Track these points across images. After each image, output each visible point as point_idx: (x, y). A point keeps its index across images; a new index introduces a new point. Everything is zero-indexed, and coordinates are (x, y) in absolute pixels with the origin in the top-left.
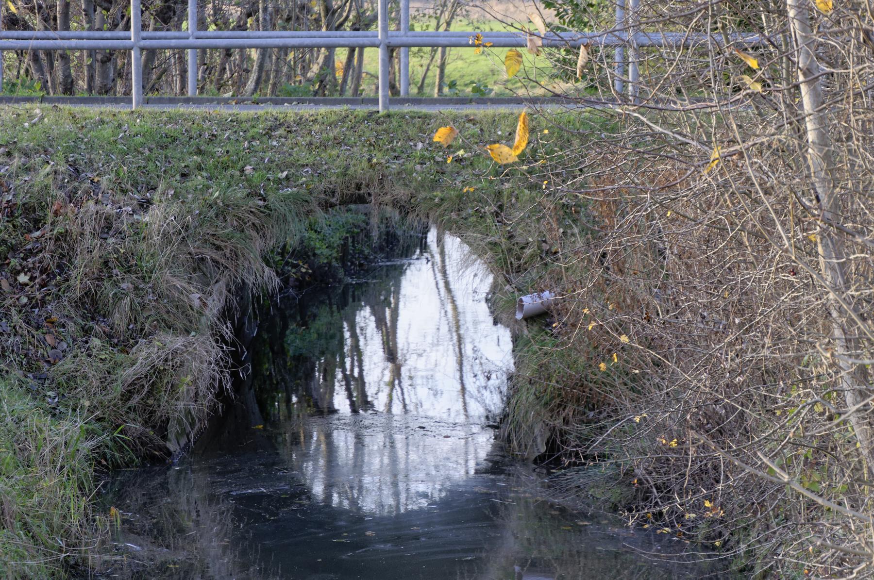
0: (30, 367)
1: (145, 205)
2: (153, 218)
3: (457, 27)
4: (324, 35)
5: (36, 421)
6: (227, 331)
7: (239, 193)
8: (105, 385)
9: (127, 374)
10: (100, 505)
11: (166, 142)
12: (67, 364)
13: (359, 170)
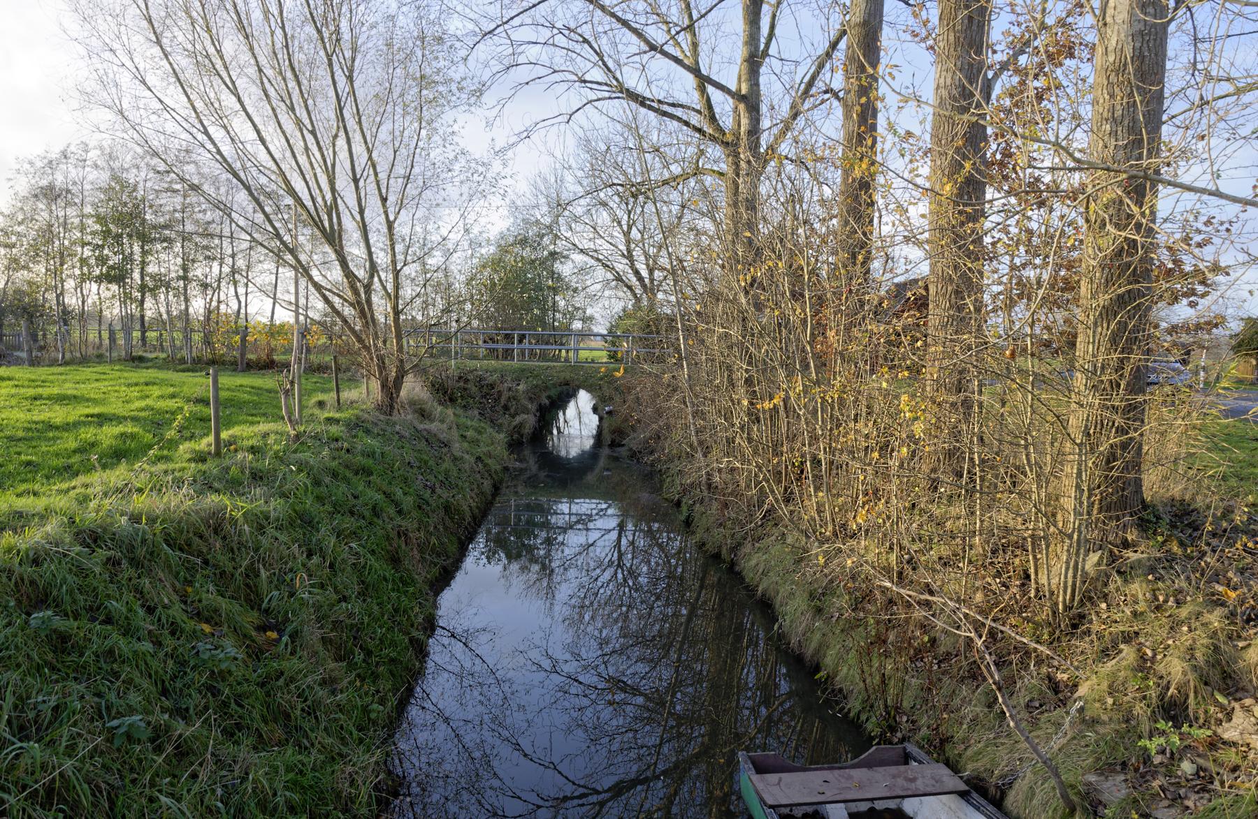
0: (492, 421)
1: (518, 385)
2: (521, 387)
3: (582, 345)
4: (554, 347)
5: (495, 434)
6: (538, 414)
7: (540, 382)
8: (509, 425)
9: (514, 423)
10: (512, 453)
11: (523, 370)
12: (500, 421)
13: (568, 378)
